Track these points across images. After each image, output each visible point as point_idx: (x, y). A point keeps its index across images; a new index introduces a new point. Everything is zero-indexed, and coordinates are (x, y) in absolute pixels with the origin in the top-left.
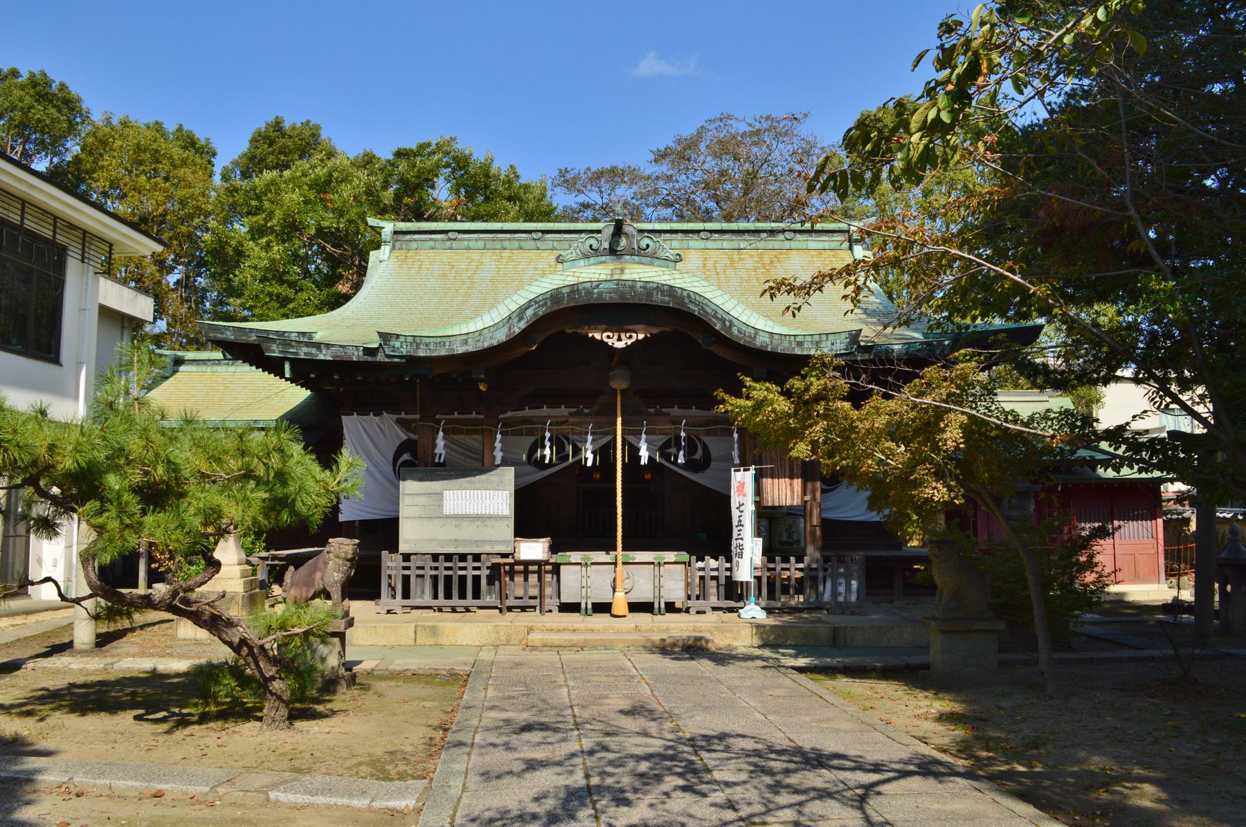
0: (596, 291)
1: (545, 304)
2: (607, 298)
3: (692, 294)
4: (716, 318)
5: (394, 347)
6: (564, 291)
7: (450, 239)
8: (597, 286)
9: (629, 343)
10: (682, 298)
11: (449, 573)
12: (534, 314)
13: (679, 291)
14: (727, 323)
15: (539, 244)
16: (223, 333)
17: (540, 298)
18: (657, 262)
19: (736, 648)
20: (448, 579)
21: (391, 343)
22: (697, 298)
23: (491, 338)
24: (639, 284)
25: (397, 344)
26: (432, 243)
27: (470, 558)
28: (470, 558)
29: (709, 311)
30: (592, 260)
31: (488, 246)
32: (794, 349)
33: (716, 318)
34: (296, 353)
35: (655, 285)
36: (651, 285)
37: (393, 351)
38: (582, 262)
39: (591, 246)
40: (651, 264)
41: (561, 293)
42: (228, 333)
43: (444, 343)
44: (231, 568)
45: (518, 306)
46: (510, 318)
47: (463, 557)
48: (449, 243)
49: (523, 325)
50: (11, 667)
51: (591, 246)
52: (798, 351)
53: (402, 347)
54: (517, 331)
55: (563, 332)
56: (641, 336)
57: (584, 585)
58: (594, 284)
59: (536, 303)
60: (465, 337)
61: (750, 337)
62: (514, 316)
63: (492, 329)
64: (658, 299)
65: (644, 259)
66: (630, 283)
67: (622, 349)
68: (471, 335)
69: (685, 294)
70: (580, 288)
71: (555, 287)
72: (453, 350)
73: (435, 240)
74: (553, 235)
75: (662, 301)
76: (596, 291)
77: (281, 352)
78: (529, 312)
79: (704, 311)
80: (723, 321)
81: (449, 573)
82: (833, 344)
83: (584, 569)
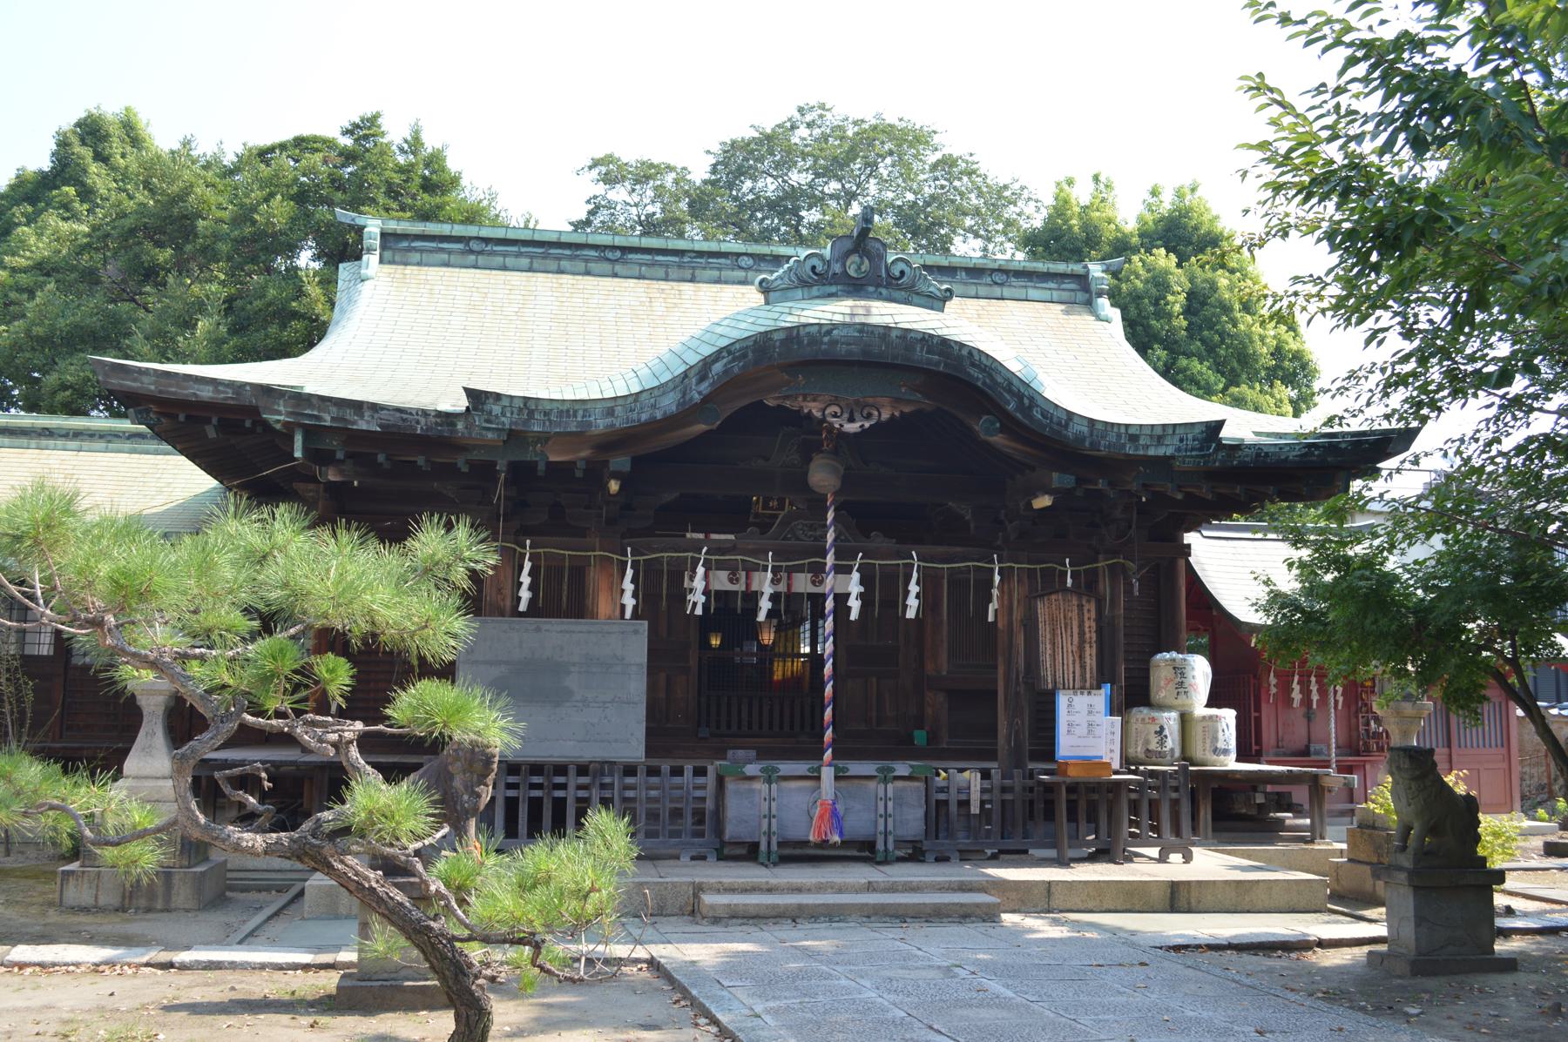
0: (826, 339)
1: (744, 356)
2: (842, 349)
3: (975, 353)
4: (1010, 391)
5: (490, 413)
6: (776, 336)
7: (472, 252)
8: (829, 332)
9: (867, 425)
10: (960, 357)
11: (536, 793)
12: (726, 372)
13: (956, 348)
14: (1026, 401)
15: (618, 268)
16: (135, 380)
17: (737, 346)
18: (916, 299)
19: (826, 928)
20: (536, 805)
21: (487, 407)
22: (983, 359)
23: (654, 406)
24: (894, 334)
25: (496, 409)
26: (445, 256)
27: (572, 771)
28: (572, 771)
29: (1000, 380)
30: (815, 291)
31: (535, 265)
32: (1124, 446)
33: (1010, 391)
34: (317, 418)
35: (920, 336)
36: (912, 335)
37: (488, 421)
38: (799, 293)
39: (813, 268)
40: (907, 302)
41: (771, 339)
42: (146, 379)
43: (575, 412)
44: (161, 783)
45: (699, 358)
46: (685, 375)
47: (561, 769)
48: (473, 257)
49: (705, 387)
50: (1562, 869)
51: (813, 268)
52: (1130, 450)
53: (503, 414)
54: (697, 398)
55: (761, 402)
56: (885, 416)
57: (881, 811)
58: (824, 329)
59: (729, 353)
60: (610, 404)
61: (1059, 424)
62: (693, 372)
63: (656, 392)
64: (920, 354)
65: (897, 294)
66: (882, 331)
67: (855, 434)
68: (620, 402)
69: (964, 352)
70: (802, 332)
71: (762, 329)
72: (589, 424)
73: (450, 252)
74: (639, 256)
75: (929, 362)
76: (826, 339)
77: (289, 414)
78: (718, 367)
79: (993, 379)
80: (1019, 396)
81: (536, 793)
82: (1181, 440)
83: (882, 786)
